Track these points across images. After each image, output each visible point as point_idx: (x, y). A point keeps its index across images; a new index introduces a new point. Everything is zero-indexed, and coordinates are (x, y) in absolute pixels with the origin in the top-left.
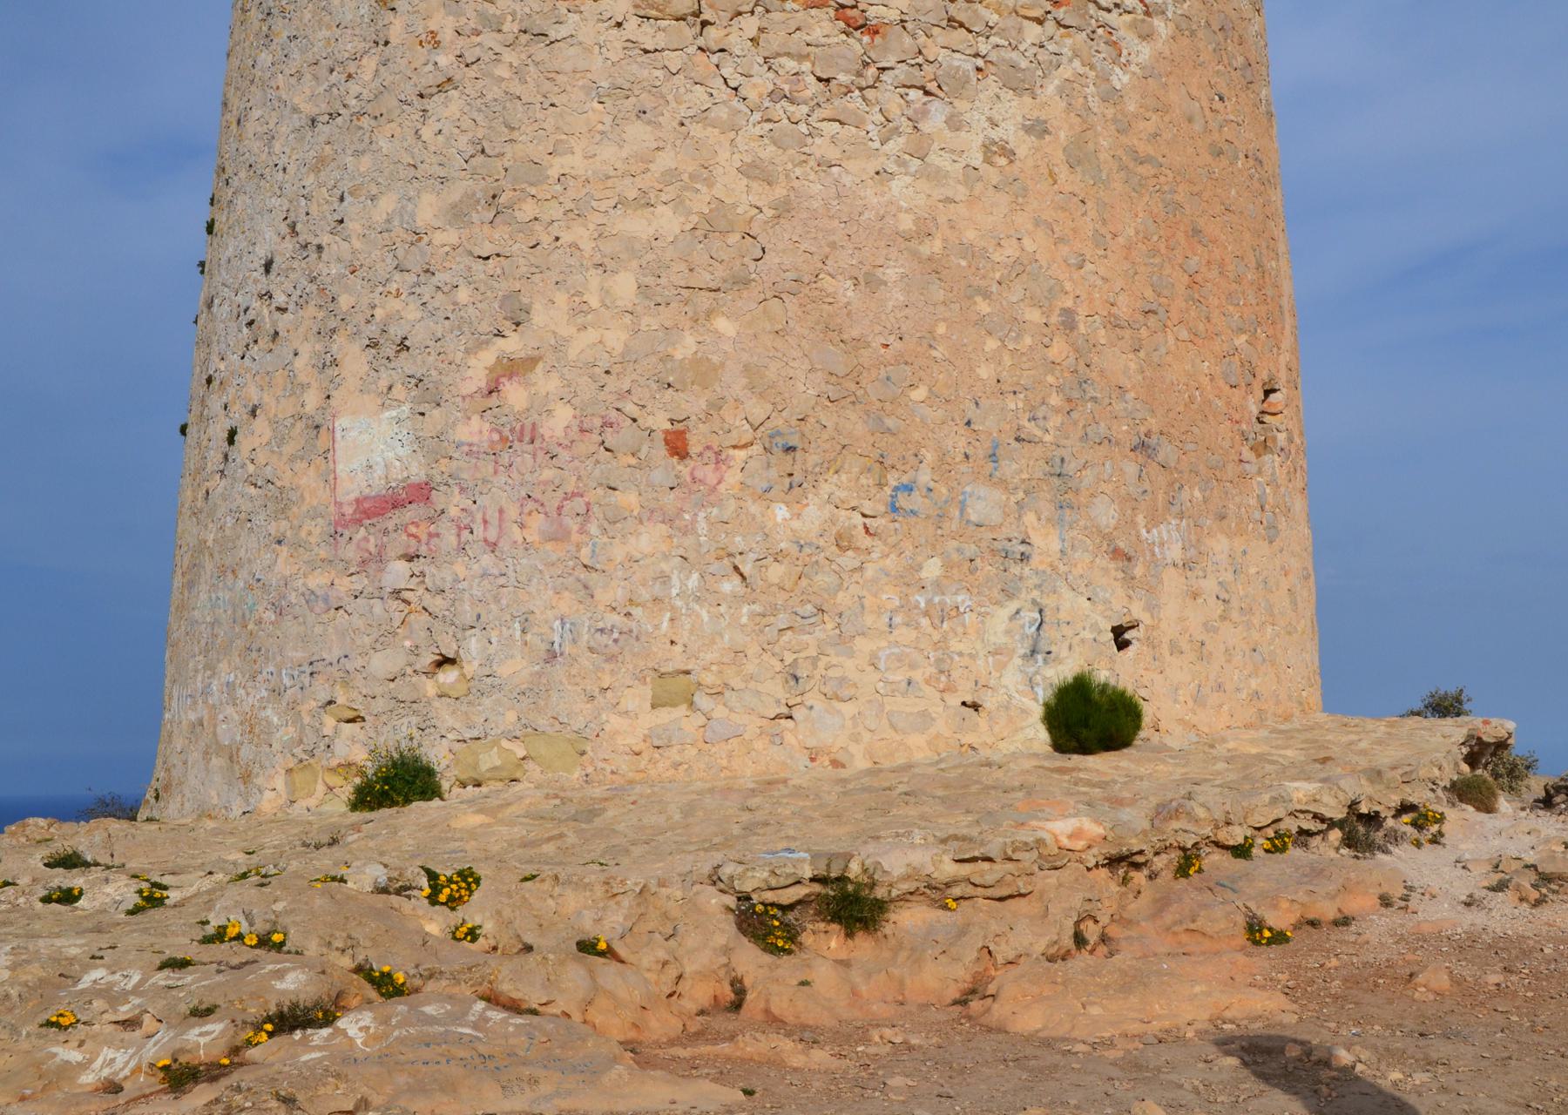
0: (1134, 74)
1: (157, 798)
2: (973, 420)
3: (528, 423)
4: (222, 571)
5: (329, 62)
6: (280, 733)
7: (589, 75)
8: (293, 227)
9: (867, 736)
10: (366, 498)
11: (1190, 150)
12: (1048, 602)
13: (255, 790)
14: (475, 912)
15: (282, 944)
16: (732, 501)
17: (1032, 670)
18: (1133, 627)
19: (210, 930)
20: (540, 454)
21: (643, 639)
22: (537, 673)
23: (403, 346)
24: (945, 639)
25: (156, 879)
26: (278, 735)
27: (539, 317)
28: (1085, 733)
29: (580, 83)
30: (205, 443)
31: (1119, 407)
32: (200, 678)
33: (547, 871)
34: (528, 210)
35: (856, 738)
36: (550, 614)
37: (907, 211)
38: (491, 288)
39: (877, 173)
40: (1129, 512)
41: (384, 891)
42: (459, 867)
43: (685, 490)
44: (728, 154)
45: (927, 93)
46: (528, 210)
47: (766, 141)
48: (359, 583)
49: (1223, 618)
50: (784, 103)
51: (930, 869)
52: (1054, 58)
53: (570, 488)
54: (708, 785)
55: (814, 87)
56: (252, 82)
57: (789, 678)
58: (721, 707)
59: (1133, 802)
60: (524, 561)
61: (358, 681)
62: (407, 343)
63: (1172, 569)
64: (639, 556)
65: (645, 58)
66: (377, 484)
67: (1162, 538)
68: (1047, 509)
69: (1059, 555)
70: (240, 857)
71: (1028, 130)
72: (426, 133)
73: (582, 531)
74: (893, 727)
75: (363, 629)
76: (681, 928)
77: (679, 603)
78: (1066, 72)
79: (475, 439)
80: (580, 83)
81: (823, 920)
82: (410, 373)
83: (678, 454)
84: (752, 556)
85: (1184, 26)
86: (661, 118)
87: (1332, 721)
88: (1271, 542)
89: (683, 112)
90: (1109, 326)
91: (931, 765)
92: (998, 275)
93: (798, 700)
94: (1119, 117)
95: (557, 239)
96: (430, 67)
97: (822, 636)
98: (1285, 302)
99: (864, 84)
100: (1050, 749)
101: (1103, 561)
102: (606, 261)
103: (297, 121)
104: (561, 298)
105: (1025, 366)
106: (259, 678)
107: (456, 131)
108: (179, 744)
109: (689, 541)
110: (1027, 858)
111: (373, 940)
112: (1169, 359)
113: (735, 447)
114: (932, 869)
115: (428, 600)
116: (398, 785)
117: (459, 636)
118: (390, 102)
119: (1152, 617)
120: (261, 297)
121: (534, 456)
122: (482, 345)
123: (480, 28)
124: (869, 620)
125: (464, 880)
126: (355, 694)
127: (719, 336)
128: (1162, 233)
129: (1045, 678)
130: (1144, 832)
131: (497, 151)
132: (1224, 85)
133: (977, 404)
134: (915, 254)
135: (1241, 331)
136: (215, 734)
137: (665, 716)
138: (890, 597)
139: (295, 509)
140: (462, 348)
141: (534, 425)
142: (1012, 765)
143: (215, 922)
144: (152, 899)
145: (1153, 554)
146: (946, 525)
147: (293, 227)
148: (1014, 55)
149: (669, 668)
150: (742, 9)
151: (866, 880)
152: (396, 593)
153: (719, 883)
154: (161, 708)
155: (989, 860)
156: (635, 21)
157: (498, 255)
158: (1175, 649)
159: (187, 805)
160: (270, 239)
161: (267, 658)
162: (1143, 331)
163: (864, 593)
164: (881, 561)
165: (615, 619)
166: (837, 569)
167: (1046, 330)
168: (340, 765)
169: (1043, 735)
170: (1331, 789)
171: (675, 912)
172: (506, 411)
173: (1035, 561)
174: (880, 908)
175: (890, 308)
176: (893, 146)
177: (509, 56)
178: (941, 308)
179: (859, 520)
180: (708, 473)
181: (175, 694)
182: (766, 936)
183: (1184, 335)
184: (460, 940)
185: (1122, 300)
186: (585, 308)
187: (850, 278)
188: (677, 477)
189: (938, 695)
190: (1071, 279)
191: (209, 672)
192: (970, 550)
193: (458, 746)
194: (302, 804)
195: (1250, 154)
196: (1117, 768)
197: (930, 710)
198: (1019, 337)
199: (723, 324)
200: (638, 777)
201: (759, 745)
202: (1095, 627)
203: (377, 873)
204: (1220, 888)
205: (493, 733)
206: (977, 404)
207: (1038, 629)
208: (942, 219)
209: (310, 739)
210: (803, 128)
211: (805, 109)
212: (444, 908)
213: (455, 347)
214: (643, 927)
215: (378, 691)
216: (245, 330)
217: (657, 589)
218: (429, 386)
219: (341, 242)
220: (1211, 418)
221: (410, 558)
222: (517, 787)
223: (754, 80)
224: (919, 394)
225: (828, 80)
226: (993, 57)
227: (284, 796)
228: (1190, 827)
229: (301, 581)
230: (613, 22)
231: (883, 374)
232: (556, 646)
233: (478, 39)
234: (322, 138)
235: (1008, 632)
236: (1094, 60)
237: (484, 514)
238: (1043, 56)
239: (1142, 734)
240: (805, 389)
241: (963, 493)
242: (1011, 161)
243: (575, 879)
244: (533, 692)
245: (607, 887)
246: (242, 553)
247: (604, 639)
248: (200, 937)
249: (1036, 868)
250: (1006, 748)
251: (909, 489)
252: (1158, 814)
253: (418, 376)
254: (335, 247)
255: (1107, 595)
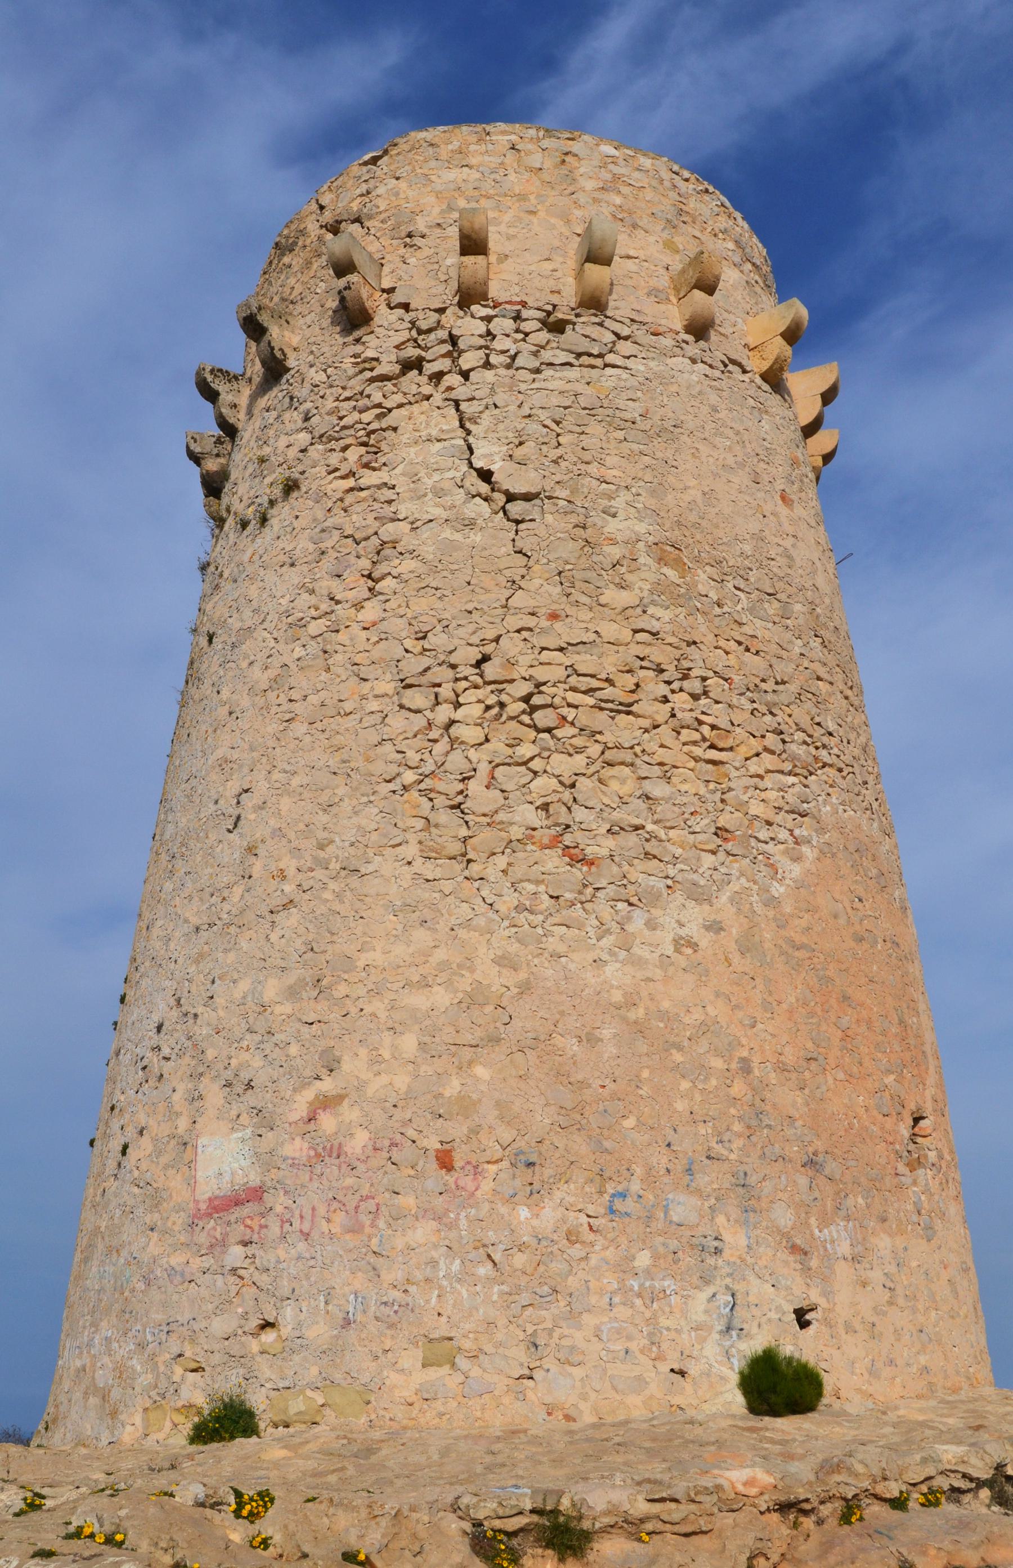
0: (789, 886)
1: (46, 1429)
2: (673, 1143)
3: (336, 1143)
4: (110, 1250)
5: (211, 890)
6: (142, 1378)
7: (387, 897)
8: (178, 1001)
9: (593, 1395)
10: (216, 1198)
11: (837, 939)
12: (739, 1287)
13: (119, 1425)
14: (269, 1526)
15: (122, 1543)
16: (486, 1204)
17: (728, 1343)
18: (812, 1310)
19: (72, 1529)
20: (344, 1166)
21: (417, 1311)
22: (335, 1336)
23: (249, 1086)
24: (655, 1316)
25: (38, 1490)
26: (140, 1380)
27: (347, 1065)
28: (773, 1398)
29: (381, 903)
30: (106, 1154)
31: (790, 1132)
32: (86, 1333)
33: (325, 1495)
34: (342, 989)
35: (584, 1397)
36: (346, 1289)
37: (617, 988)
38: (314, 1045)
39: (595, 961)
40: (803, 1215)
41: (202, 1505)
42: (259, 1489)
43: (451, 1195)
44: (485, 950)
45: (631, 904)
46: (342, 989)
47: (513, 940)
48: (208, 1262)
49: (891, 1303)
50: (526, 913)
51: (626, 1506)
52: (726, 878)
53: (365, 1193)
54: (465, 1433)
55: (546, 902)
56: (159, 901)
57: (530, 1345)
58: (476, 1368)
59: (802, 1457)
60: (329, 1248)
61: (202, 1340)
62: (252, 1084)
63: (843, 1262)
64: (415, 1245)
65: (427, 885)
66: (224, 1187)
67: (832, 1237)
68: (735, 1213)
69: (746, 1249)
70: (100, 1476)
71: (708, 928)
72: (274, 937)
73: (373, 1225)
74: (615, 1388)
75: (208, 1298)
76: (427, 1547)
77: (445, 1283)
78: (734, 886)
79: (297, 1155)
80: (381, 903)
81: (541, 1547)
82: (253, 1105)
83: (445, 1167)
84: (502, 1247)
85: (826, 850)
86: (437, 926)
87: (997, 1394)
88: (929, 1241)
89: (453, 921)
90: (778, 1070)
91: (645, 1421)
92: (688, 1034)
93: (538, 1364)
94: (778, 916)
95: (362, 1010)
96: (279, 893)
97: (556, 1312)
98: (927, 1048)
99: (584, 899)
100: (746, 1411)
101: (783, 1255)
102: (396, 1025)
103: (186, 928)
104: (363, 1052)
105: (713, 1101)
106: (130, 1335)
107: (295, 936)
108: (66, 1385)
109: (453, 1234)
110: (708, 1500)
111: (189, 1542)
112: (830, 1094)
113: (488, 1162)
114: (629, 1506)
115: (257, 1277)
116: (227, 1423)
117: (278, 1305)
118: (250, 916)
119: (828, 1302)
120: (153, 1049)
121: (340, 1167)
122: (305, 1085)
123: (314, 867)
124: (593, 1300)
125: (263, 1500)
126: (198, 1350)
127: (478, 1079)
128: (818, 999)
129: (739, 1351)
130: (810, 1483)
131: (322, 949)
132: (862, 890)
133: (675, 1130)
134: (625, 1020)
135: (889, 1072)
136: (93, 1378)
137: (433, 1373)
138: (610, 1281)
139: (165, 1204)
140: (291, 1088)
141: (340, 1144)
142: (711, 1424)
143: (76, 1523)
144: (33, 1505)
145: (826, 1250)
146: (653, 1224)
147: (178, 1001)
148: (695, 876)
149: (435, 1335)
150: (495, 851)
151: (574, 1514)
152: (234, 1271)
153: (458, 1511)
154: (58, 1357)
155: (675, 1500)
156: (421, 860)
157: (319, 1022)
158: (850, 1329)
159: (68, 1435)
160: (162, 1009)
161: (136, 1319)
162: (807, 1074)
163: (590, 1278)
164: (603, 1253)
165: (396, 1294)
166: (568, 1258)
167: (727, 1074)
168: (184, 1406)
169: (739, 1399)
170: (977, 1453)
171: (423, 1534)
172: (320, 1133)
173: (727, 1253)
174: (586, 1538)
175: (606, 1058)
176: (607, 941)
177: (332, 885)
178: (646, 1058)
179: (584, 1220)
180: (468, 1182)
181: (68, 1345)
182: (494, 1557)
183: (841, 1076)
184: (255, 1548)
185: (788, 1050)
186: (380, 1059)
187: (576, 1037)
188: (445, 1185)
189: (651, 1362)
190: (746, 1036)
191: (93, 1329)
192: (674, 1244)
193: (273, 1394)
194: (154, 1436)
195: (887, 939)
196: (800, 1429)
197: (645, 1375)
198: (707, 1079)
199: (481, 1072)
200: (411, 1423)
201: (506, 1400)
202: (779, 1309)
203: (198, 1491)
204: (879, 1535)
205: (300, 1383)
206: (675, 1130)
207: (732, 1309)
208: (644, 994)
209: (163, 1384)
210: (540, 931)
211: (541, 918)
212: (246, 1521)
213: (286, 1087)
214: (395, 1545)
215: (216, 1347)
216: (140, 1073)
217: (428, 1272)
218: (267, 1115)
219: (211, 1012)
220: (868, 1140)
221: (245, 1244)
222: (317, 1429)
223: (504, 898)
224: (630, 1122)
225: (557, 897)
226: (679, 878)
227: (141, 1430)
228: (850, 1480)
229: (165, 1260)
230: (405, 861)
231: (601, 1108)
232: (351, 1314)
233: (312, 874)
234: (202, 941)
235: (706, 1312)
236: (757, 877)
237: (301, 1211)
238: (717, 876)
239: (825, 1401)
240: (542, 1119)
241: (666, 1199)
242: (695, 951)
243: (346, 1502)
244: (331, 1352)
245: (369, 1510)
246: (125, 1237)
247: (387, 1310)
248: (63, 1534)
249: (715, 1510)
250: (709, 1409)
251: (623, 1195)
252: (822, 1467)
253: (259, 1107)
254: (206, 1015)
255: (789, 1283)
